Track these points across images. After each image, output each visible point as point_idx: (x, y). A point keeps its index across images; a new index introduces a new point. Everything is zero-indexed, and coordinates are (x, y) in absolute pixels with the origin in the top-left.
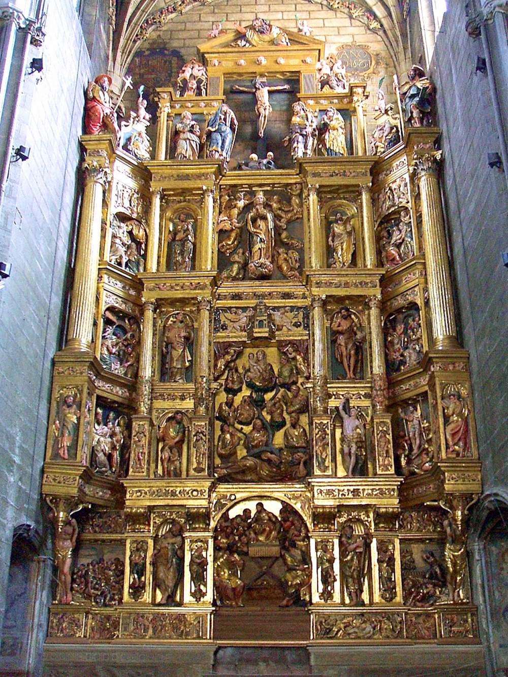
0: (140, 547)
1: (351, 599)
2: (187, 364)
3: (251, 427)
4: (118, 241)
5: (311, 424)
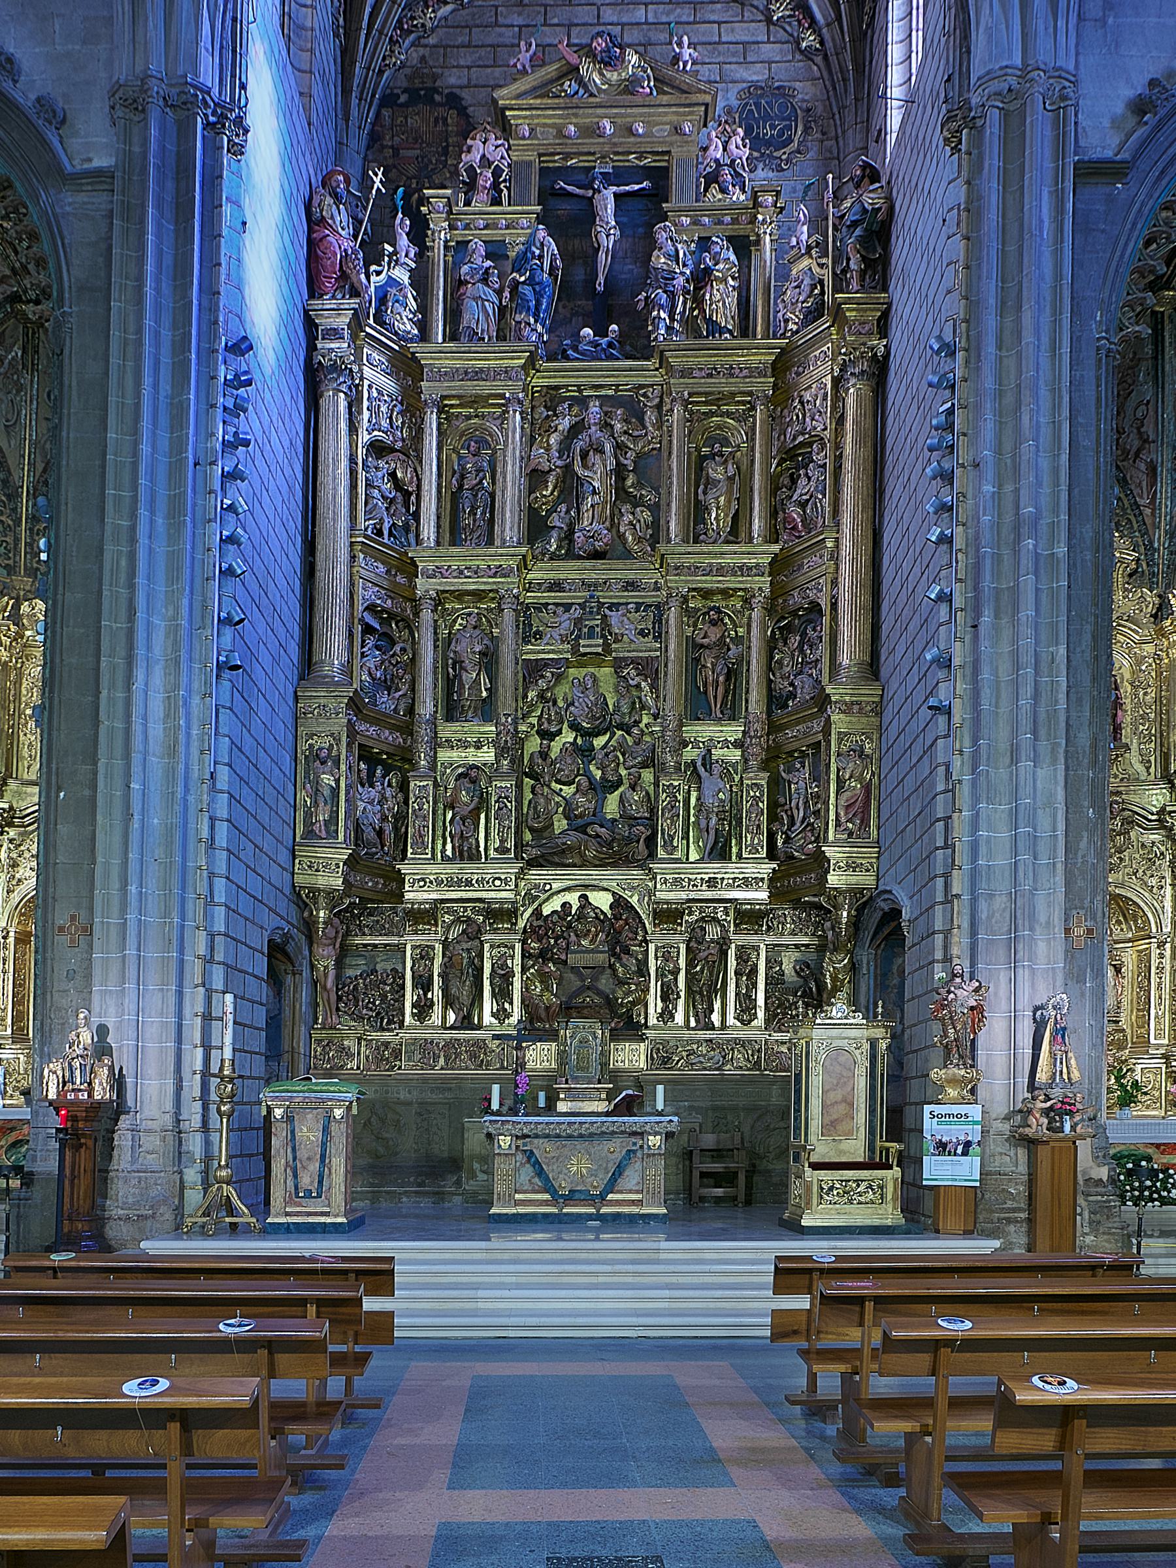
0: (425, 954)
1: (697, 1021)
2: (484, 694)
3: (573, 789)
4: (376, 493)
5: (656, 784)
